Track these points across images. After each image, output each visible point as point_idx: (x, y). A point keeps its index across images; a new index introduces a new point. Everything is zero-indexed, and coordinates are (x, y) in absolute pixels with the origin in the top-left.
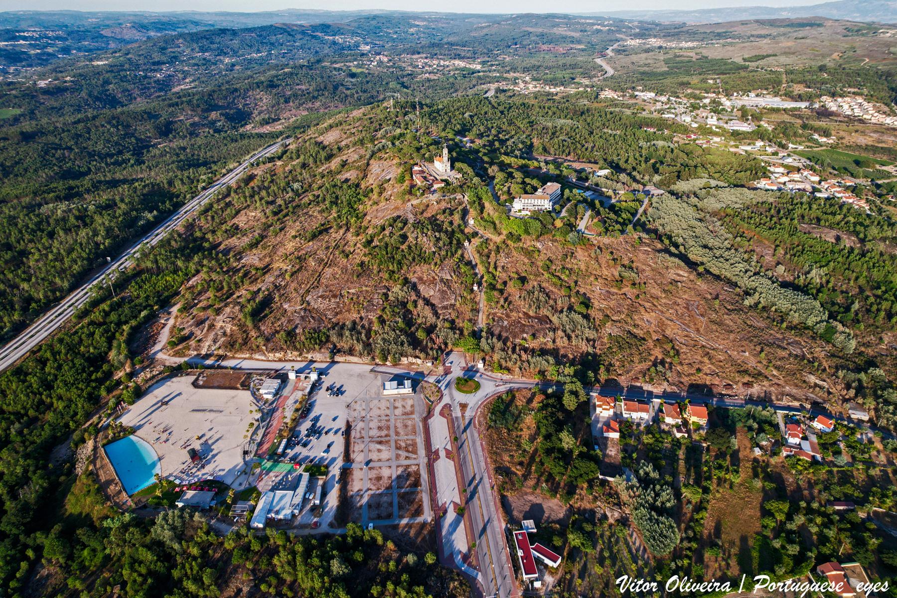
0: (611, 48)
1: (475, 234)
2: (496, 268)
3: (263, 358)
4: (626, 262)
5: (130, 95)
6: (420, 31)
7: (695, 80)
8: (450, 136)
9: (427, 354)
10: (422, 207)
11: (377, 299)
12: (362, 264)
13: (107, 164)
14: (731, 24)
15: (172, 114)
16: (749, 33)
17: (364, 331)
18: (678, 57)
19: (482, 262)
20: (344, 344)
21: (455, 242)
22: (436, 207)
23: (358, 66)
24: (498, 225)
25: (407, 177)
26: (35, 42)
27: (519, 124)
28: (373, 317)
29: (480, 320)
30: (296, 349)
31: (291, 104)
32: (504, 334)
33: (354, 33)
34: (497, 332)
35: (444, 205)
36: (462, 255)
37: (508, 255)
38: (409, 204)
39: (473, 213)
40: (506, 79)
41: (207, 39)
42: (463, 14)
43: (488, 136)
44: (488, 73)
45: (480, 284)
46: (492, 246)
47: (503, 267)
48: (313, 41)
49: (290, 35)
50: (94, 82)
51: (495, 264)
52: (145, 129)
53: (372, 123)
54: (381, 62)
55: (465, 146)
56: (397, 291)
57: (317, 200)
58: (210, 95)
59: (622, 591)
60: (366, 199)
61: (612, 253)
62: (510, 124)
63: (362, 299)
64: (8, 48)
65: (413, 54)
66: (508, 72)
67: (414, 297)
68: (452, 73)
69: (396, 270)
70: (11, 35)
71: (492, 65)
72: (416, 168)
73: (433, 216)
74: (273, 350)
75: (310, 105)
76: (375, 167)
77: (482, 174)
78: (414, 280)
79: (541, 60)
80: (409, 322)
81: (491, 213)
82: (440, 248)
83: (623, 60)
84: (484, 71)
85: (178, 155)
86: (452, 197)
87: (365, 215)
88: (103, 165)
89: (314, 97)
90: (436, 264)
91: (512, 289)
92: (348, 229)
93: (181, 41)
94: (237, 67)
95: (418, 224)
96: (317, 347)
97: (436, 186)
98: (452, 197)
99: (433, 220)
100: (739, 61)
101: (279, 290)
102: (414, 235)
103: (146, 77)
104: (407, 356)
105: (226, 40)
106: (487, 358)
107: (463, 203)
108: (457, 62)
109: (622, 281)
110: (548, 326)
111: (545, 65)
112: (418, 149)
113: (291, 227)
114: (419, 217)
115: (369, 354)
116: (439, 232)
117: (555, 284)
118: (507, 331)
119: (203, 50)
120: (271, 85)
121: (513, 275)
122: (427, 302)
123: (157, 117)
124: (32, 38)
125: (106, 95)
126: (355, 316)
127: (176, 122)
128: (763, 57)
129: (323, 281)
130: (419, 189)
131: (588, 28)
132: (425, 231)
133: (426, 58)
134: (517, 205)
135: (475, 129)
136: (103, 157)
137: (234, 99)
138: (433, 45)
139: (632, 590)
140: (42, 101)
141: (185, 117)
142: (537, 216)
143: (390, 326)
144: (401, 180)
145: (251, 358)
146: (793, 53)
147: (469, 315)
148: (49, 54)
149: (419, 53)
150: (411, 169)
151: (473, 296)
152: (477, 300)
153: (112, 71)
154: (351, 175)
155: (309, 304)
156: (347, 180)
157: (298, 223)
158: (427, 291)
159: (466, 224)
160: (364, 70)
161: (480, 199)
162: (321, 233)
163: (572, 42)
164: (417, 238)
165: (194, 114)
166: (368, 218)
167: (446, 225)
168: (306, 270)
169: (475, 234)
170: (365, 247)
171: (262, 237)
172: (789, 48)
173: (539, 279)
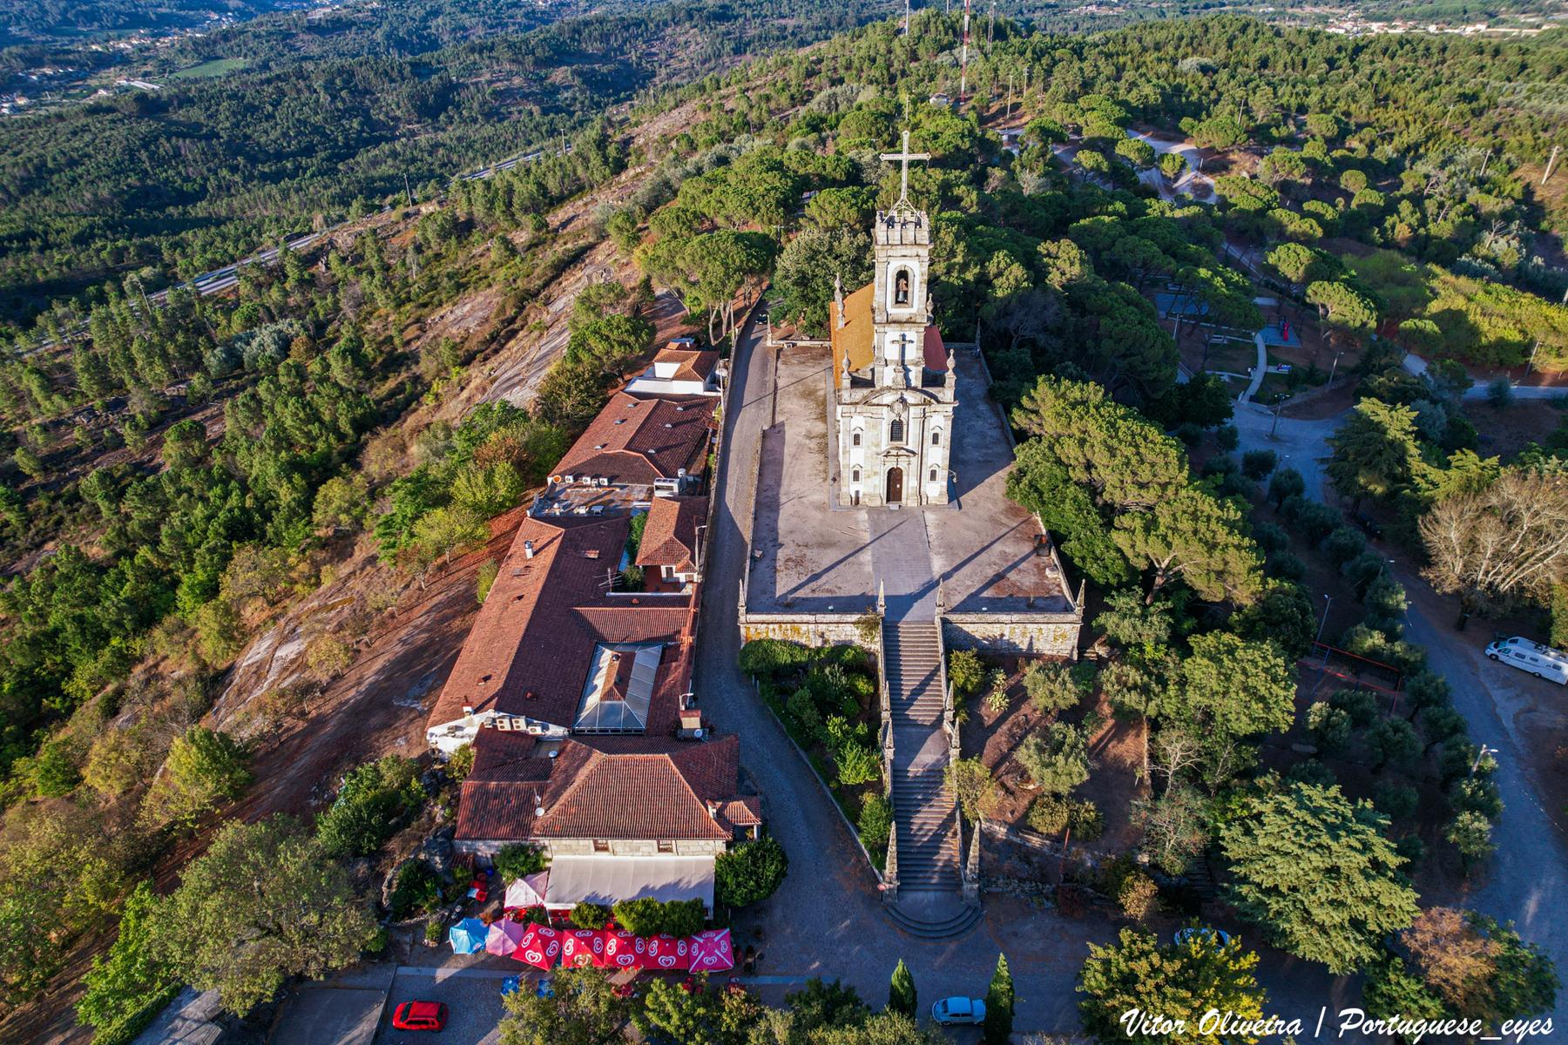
4: (776, 33)
7: (401, 195)
8: (1096, 125)
43: (1292, 142)
59: (1130, 1034)
62: (1382, 101)
125: (421, 37)
139: (1145, 1032)
140: (299, 44)
165: (515, 68)
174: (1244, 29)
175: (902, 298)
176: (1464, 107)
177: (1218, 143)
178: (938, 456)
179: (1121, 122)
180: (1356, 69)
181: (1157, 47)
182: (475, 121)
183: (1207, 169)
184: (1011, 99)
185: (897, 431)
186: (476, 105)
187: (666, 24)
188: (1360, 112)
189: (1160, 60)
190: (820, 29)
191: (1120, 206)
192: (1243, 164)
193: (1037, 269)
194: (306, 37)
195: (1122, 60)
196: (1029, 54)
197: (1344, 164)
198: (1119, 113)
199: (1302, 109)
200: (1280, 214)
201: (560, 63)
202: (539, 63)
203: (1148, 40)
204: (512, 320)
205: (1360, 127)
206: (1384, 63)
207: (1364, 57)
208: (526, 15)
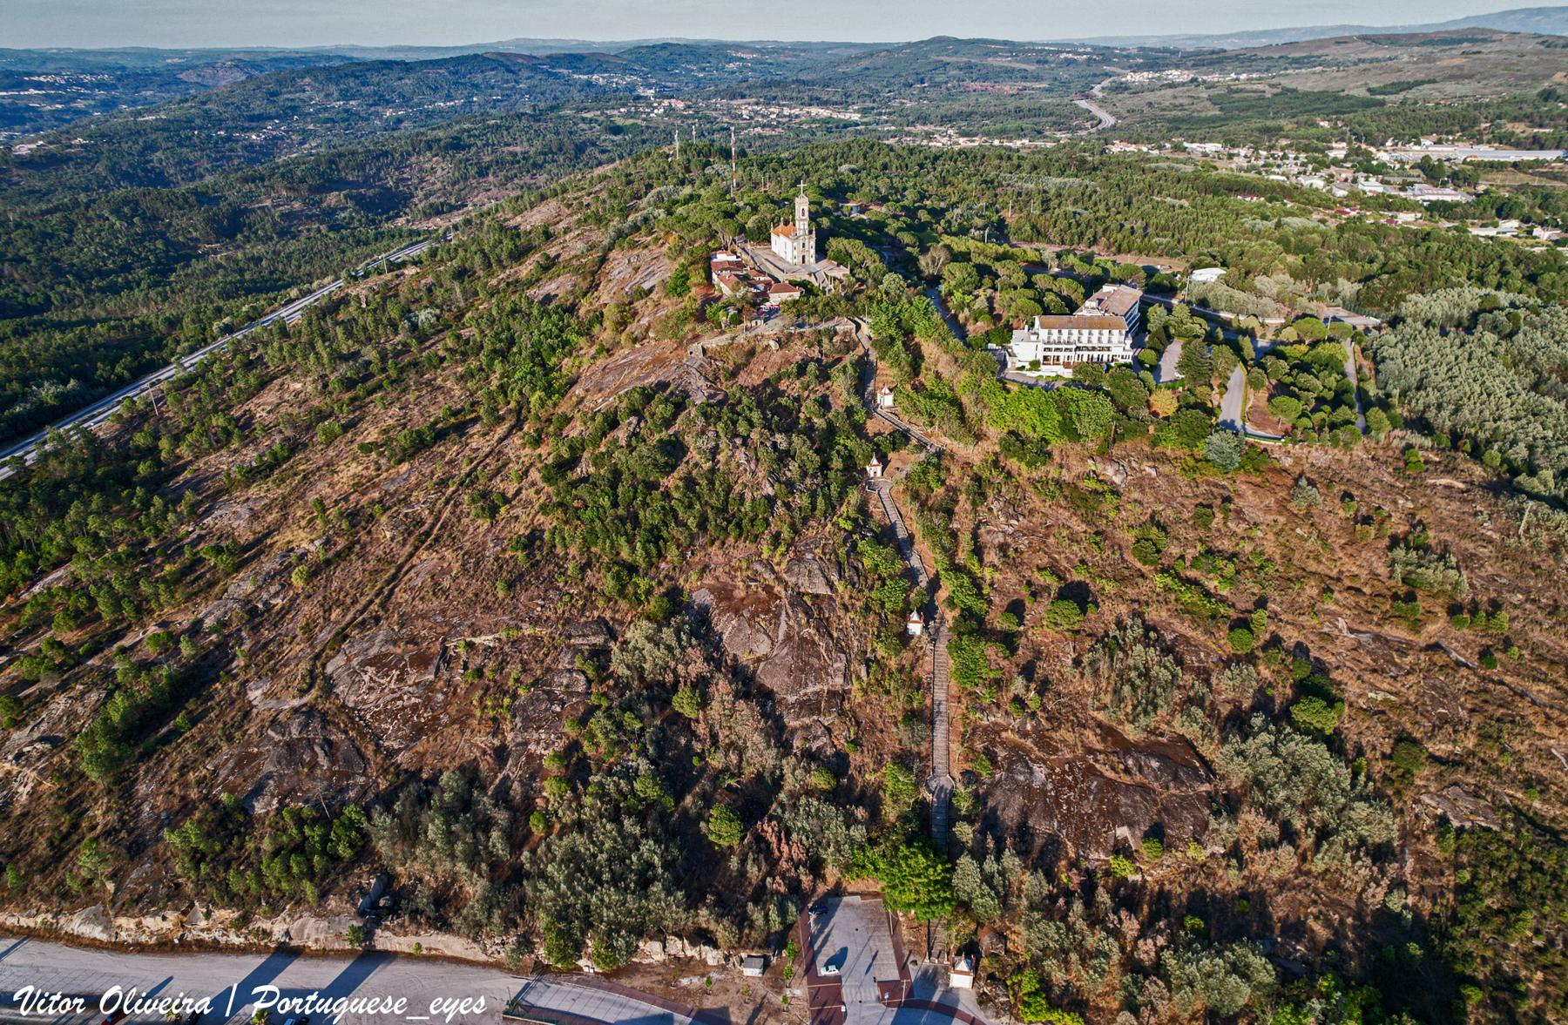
0: (1098, 87)
1: (900, 438)
2: (978, 551)
3: (97, 932)
4: (509, 158)
5: (193, 170)
9: (742, 921)
11: (570, 676)
12: (532, 541)
13: (88, 292)
14: (1321, 44)
15: (250, 197)
16: (1353, 57)
17: (502, 816)
18: (1237, 91)
19: (931, 531)
20: (424, 866)
21: (837, 463)
23: (628, 115)
24: (971, 410)
25: (696, 278)
26: (54, 92)
28: (545, 748)
29: (939, 758)
30: (231, 899)
31: (491, 178)
32: (1042, 827)
33: (626, 70)
34: (1010, 816)
35: (799, 350)
36: (862, 508)
37: (1014, 508)
38: (696, 347)
39: (888, 373)
40: (908, 134)
41: (357, 77)
45: (928, 612)
46: (956, 476)
47: (1003, 548)
48: (551, 80)
49: (509, 71)
50: (125, 146)
51: (975, 536)
52: (189, 225)
53: (629, 183)
54: (670, 111)
56: (641, 644)
57: (465, 350)
58: (331, 162)
60: (582, 341)
61: (1347, 496)
63: (514, 670)
64: (6, 102)
65: (733, 97)
66: (913, 124)
67: (698, 667)
69: (641, 562)
70: (16, 81)
71: (880, 114)
72: (722, 257)
73: (767, 382)
74: (139, 903)
75: (527, 179)
76: (620, 265)
78: (703, 597)
80: (677, 771)
81: (946, 374)
82: (790, 485)
83: (1127, 101)
84: (866, 124)
85: (241, 271)
86: (823, 326)
87: (573, 382)
88: (79, 291)
89: (535, 165)
90: (776, 539)
91: (1046, 627)
92: (518, 425)
93: (307, 80)
94: (405, 124)
95: (721, 409)
96: (309, 889)
97: (775, 299)
98: (823, 326)
99: (767, 395)
100: (1362, 93)
101: (255, 629)
102: (706, 443)
103: (229, 139)
104: (660, 935)
105: (391, 79)
106: (986, 941)
107: (856, 344)
108: (814, 111)
109: (1410, 597)
110: (1204, 788)
112: (729, 215)
113: (375, 422)
114: (724, 385)
115: (509, 923)
116: (788, 431)
117: (1186, 611)
118: (1049, 815)
119: (346, 95)
120: (456, 145)
121: (1042, 579)
122: (748, 686)
123: (214, 201)
124: (51, 85)
125: (145, 170)
126: (476, 743)
127: (254, 210)
128: (1410, 86)
129: (401, 596)
130: (725, 307)
131: (1050, 58)
132: (742, 428)
134: (1024, 349)
136: (82, 276)
137: (379, 169)
138: (770, 84)
140: (15, 179)
141: (273, 202)
142: (1090, 376)
143: (602, 794)
144: (679, 285)
145: (49, 934)
146: (1471, 77)
147: (899, 736)
148: (78, 112)
149: (743, 97)
150: (709, 259)
151: (907, 656)
152: (923, 671)
153: (164, 130)
154: (559, 286)
155: (329, 686)
156: (548, 299)
157: (395, 410)
158: (747, 642)
159: (870, 405)
161: (908, 333)
162: (440, 436)
163: (1025, 78)
164: (715, 451)
165: (292, 194)
166: (578, 391)
167: (808, 410)
168: (363, 556)
169: (900, 438)
170: (547, 479)
171: (293, 447)
172: (1460, 68)
173: (1131, 592)
174: (872, 147)
178: (813, 251)
181: (824, 160)
182: (271, 239)
186: (268, 226)
187: (409, 154)
194: (22, 173)
197: (920, 208)
199: (905, 189)
201: (330, 190)
202: (314, 190)
203: (817, 156)
206: (949, 165)
208: (245, 147)
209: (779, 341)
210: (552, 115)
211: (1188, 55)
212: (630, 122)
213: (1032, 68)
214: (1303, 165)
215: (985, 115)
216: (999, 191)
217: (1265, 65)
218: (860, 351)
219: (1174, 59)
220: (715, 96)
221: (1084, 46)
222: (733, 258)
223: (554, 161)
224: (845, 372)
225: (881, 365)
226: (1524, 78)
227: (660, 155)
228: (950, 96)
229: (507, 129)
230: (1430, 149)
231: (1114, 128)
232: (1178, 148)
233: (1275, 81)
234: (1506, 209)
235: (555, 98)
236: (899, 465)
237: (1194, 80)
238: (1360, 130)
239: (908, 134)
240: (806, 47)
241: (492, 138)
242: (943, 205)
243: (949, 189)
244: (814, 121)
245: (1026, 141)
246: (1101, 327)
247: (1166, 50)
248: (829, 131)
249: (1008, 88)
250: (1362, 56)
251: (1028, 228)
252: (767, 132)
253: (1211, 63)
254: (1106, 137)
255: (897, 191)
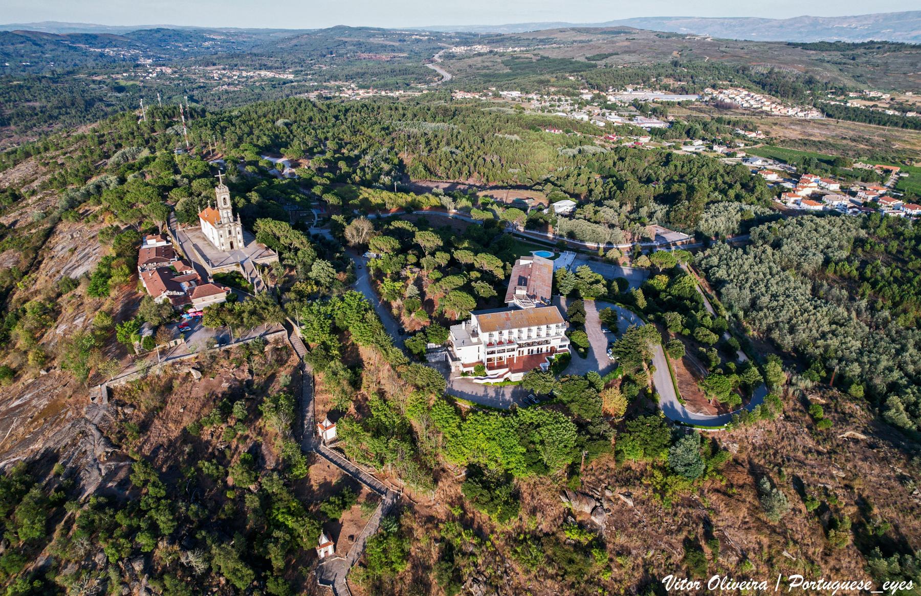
0: (437, 56)
6: (217, 45)
8: (249, 156)
10: (147, 400)
14: (552, 31)
16: (570, 39)
18: (517, 58)
22: (199, 386)
23: (129, 78)
27: (368, 132)
31: (13, 127)
33: (130, 46)
35: (226, 376)
39: (328, 392)
40: (326, 88)
42: (267, 29)
43: (323, 152)
44: (303, 83)
48: (71, 52)
54: (161, 75)
55: (280, 173)
62: (355, 133)
65: (207, 65)
66: (328, 80)
68: (257, 84)
71: (307, 75)
73: (186, 435)
77: (331, 247)
79: (364, 67)
83: (456, 65)
89: (51, 117)
97: (200, 304)
100: (582, 59)
108: (263, 73)
111: (370, 71)
131: (407, 38)
133: (224, 69)
135: (296, 142)
146: (634, 52)
149: (214, 65)
160: (138, 83)
163: (393, 51)
169: (348, 488)
174: (300, 104)
175: (225, 203)
176: (383, 132)
177: (295, 157)
178: (240, 237)
179: (258, 154)
180: (347, 119)
181: (265, 116)
183: (292, 167)
184: (211, 148)
185: (230, 232)
188: (347, 137)
189: (267, 122)
190: (60, 108)
191: (265, 182)
192: (305, 163)
193: (248, 200)
195: (251, 123)
196: (209, 126)
197: (339, 159)
198: (256, 150)
199: (326, 139)
200: (315, 179)
203: (260, 113)
204: (35, 258)
205: (346, 144)
207: (349, 114)
209: (200, 369)
210: (67, 78)
211: (483, 37)
212: (131, 83)
213: (397, 44)
214: (572, 105)
215: (373, 75)
216: (394, 135)
217: (526, 42)
218: (294, 360)
219: (476, 39)
220: (195, 64)
221: (424, 31)
222: (164, 243)
223: (67, 113)
224: (277, 409)
225: (320, 377)
226: (660, 54)
227: (132, 118)
228: (350, 63)
229: (28, 89)
230: (629, 94)
231: (451, 81)
232: (496, 95)
233: (535, 52)
234: (692, 133)
235: (75, 65)
236: (352, 530)
237: (491, 52)
238: (592, 82)
239: (326, 88)
240: (257, 32)
241: (13, 95)
242: (356, 152)
243: (359, 137)
244: (263, 80)
245: (402, 92)
246: (539, 323)
247: (470, 34)
248: (274, 87)
249: (384, 57)
250: (575, 39)
251: (421, 168)
252: (232, 88)
253: (497, 42)
254: (450, 86)
255: (320, 141)
